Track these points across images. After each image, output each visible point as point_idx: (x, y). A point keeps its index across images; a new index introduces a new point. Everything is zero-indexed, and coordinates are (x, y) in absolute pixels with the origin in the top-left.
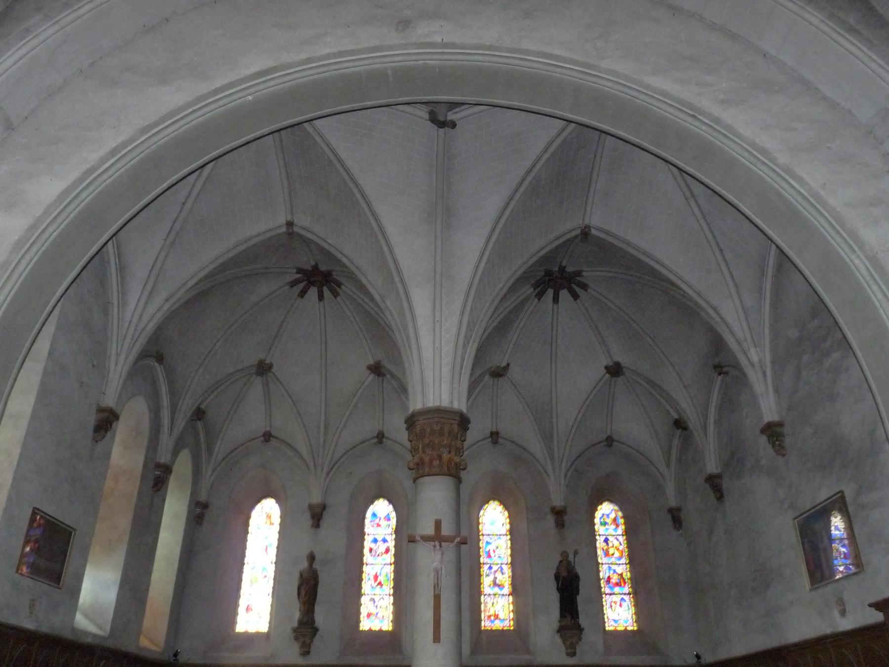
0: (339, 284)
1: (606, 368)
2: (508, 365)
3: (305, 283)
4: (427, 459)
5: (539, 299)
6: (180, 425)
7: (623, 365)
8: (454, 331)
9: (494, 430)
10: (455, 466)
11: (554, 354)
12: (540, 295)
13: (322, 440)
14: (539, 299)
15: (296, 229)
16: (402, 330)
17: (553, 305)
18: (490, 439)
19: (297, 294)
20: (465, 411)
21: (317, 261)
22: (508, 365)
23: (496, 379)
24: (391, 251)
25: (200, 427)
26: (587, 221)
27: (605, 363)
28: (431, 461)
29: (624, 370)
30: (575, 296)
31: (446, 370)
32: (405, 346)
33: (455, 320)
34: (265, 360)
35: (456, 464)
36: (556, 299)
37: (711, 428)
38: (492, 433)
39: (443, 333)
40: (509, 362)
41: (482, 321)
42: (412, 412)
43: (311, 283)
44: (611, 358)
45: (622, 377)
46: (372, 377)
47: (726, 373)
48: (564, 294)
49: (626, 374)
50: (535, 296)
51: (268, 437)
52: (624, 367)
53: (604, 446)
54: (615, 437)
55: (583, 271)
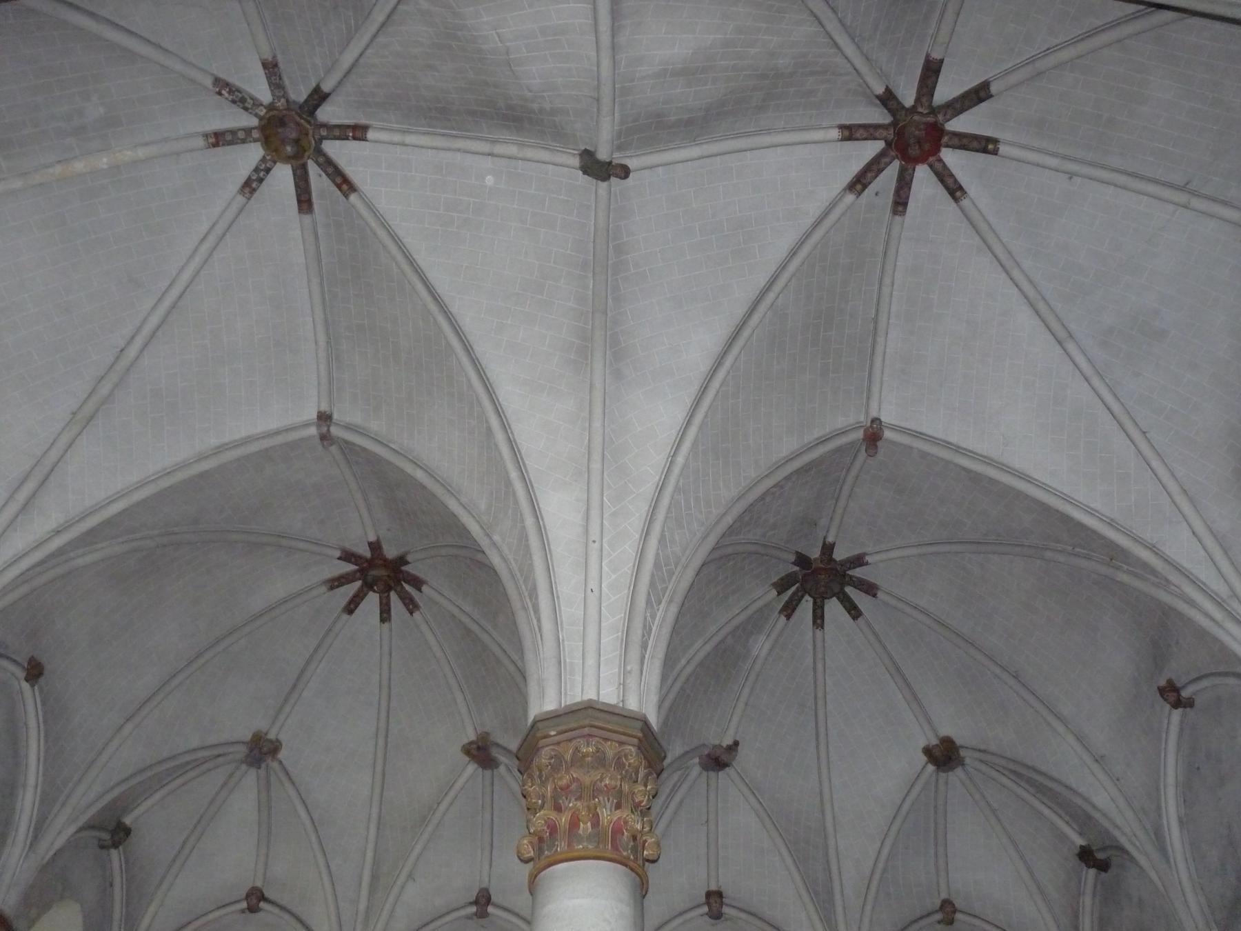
0: (417, 583)
1: (928, 751)
2: (736, 744)
3: (358, 584)
4: (564, 820)
5: (788, 617)
6: (61, 832)
7: (958, 742)
8: (628, 568)
9: (713, 887)
10: (632, 843)
11: (822, 736)
12: (789, 609)
13: (363, 905)
14: (788, 617)
15: (334, 431)
16: (521, 582)
17: (814, 632)
18: (706, 909)
19: (340, 610)
20: (653, 719)
21: (381, 537)
22: (736, 744)
23: (712, 774)
24: (505, 427)
25: (116, 864)
26: (874, 414)
27: (922, 743)
28: (574, 823)
29: (962, 753)
30: (854, 611)
31: (610, 641)
32: (525, 609)
33: (629, 549)
34: (266, 734)
35: (634, 838)
36: (818, 619)
37: (1175, 836)
38: (709, 894)
39: (605, 568)
40: (737, 739)
41: (685, 567)
42: (534, 719)
43: (369, 586)
44: (934, 730)
45: (959, 771)
46: (472, 768)
47: (1190, 703)
48: (833, 608)
49: (968, 761)
50: (780, 612)
51: (256, 899)
52: (962, 747)
53: (939, 922)
54: (959, 903)
55: (867, 554)
